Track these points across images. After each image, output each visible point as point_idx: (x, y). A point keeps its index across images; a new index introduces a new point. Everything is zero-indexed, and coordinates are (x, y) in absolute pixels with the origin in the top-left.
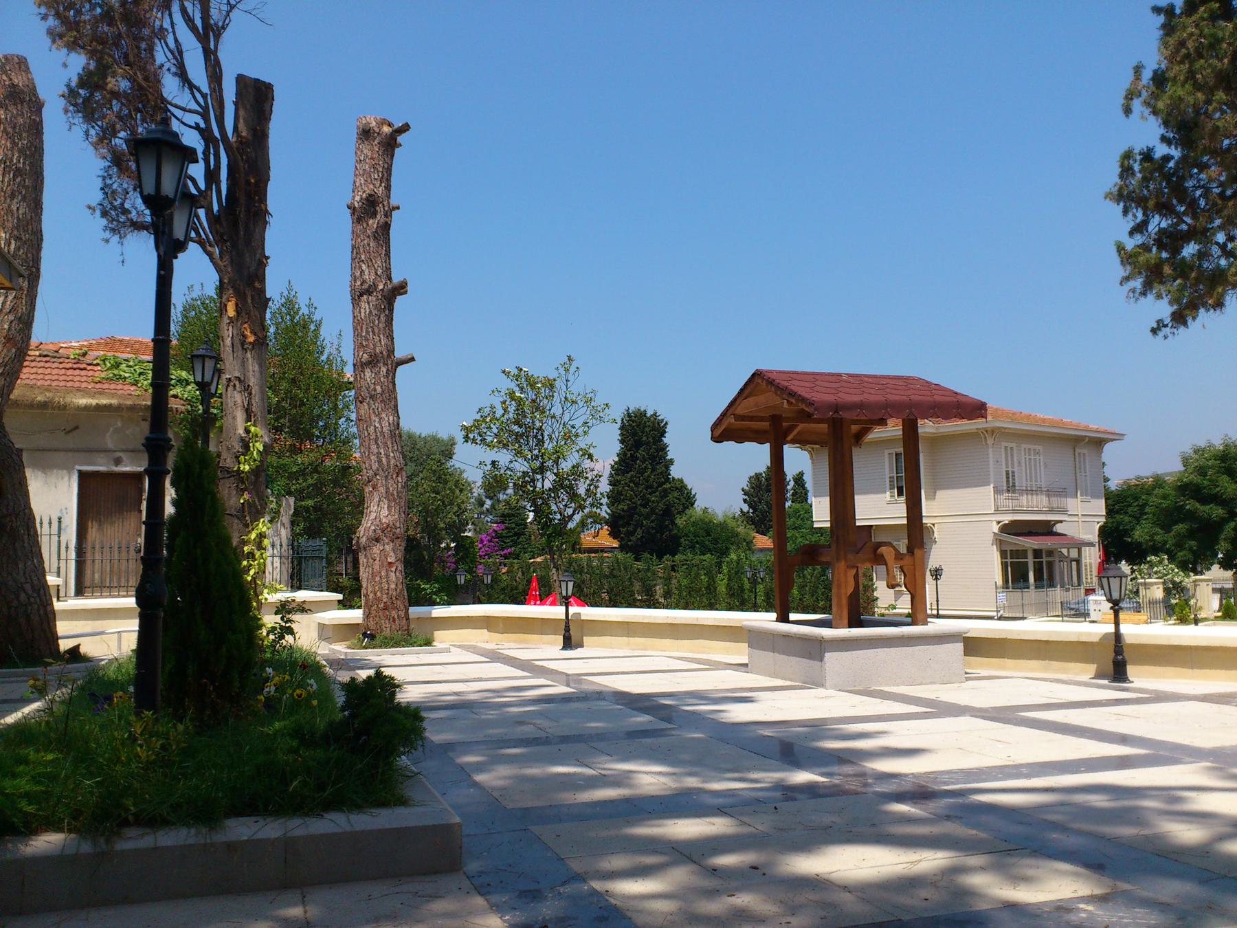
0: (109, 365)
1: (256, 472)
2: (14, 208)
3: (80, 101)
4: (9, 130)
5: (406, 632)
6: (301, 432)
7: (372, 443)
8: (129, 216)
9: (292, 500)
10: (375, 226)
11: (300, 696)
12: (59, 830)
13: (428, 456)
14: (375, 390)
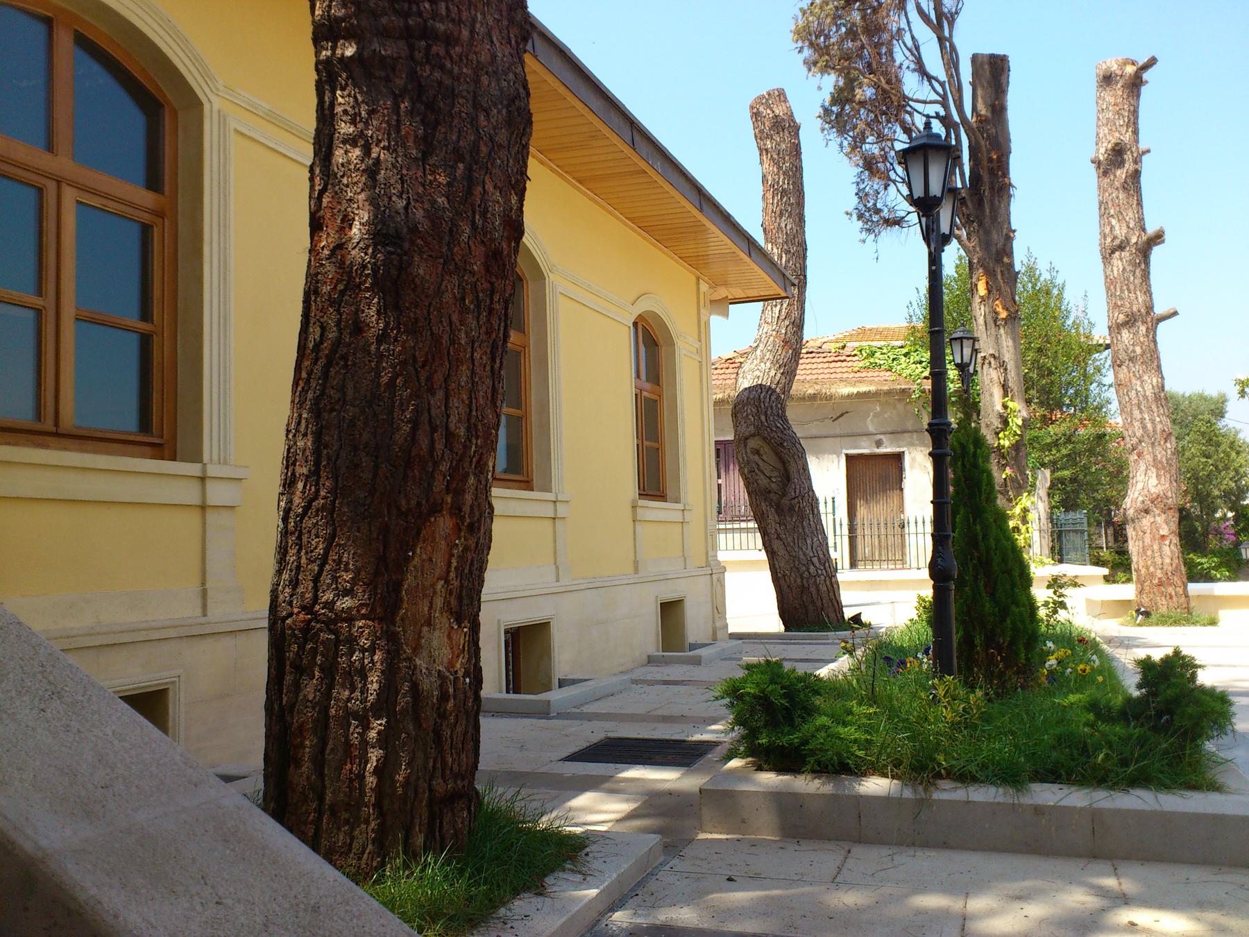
0: (865, 355)
1: (1017, 447)
2: (783, 225)
3: (833, 117)
4: (775, 156)
5: (1186, 610)
6: (1051, 402)
7: (1135, 408)
8: (882, 215)
9: (1048, 473)
10: (1124, 176)
11: (1084, 671)
12: (884, 775)
13: (1195, 417)
14: (1134, 351)
